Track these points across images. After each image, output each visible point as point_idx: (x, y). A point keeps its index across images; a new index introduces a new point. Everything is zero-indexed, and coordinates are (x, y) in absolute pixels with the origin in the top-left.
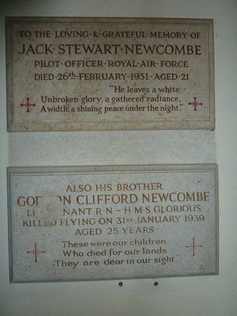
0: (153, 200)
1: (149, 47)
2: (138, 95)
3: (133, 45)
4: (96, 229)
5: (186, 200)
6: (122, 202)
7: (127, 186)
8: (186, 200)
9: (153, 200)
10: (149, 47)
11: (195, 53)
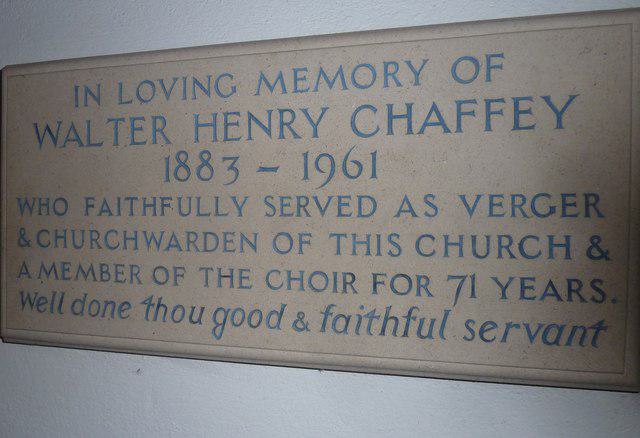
0: (63, 276)
1: (86, 276)
2: (56, 304)
3: (270, 112)
4: (360, 198)
5: (213, 79)
6: (419, 294)
7: (511, 243)
8: (213, 79)
9: (63, 276)
10: (86, 276)
11: (113, 278)
